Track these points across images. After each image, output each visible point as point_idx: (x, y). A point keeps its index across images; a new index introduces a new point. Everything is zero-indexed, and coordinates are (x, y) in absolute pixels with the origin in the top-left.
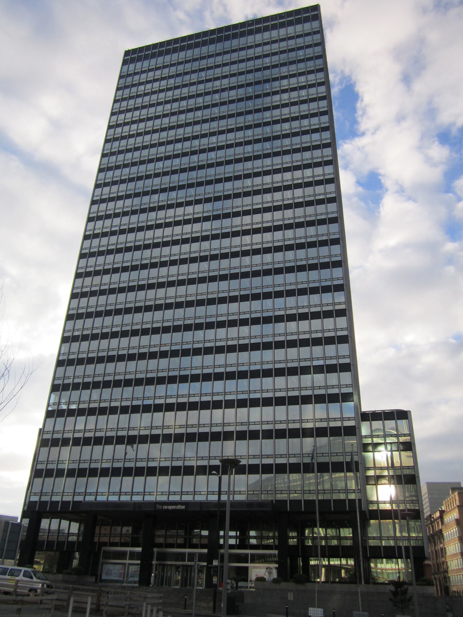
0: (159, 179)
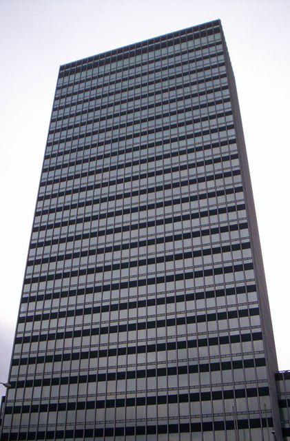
0: (94, 162)
